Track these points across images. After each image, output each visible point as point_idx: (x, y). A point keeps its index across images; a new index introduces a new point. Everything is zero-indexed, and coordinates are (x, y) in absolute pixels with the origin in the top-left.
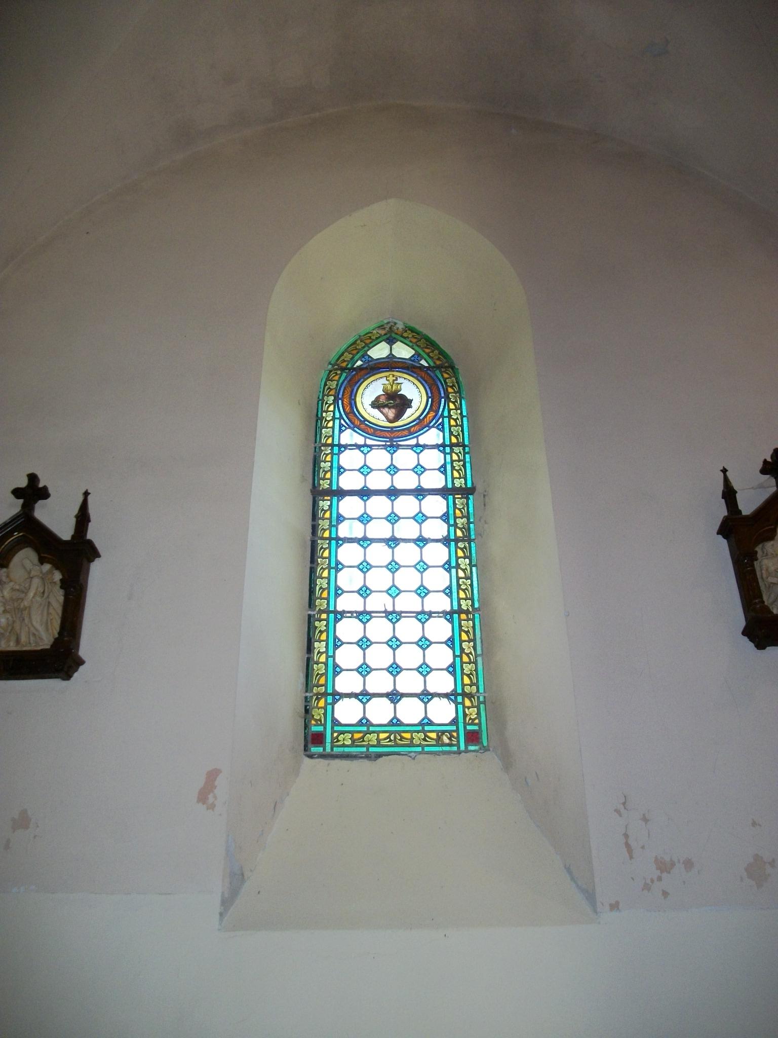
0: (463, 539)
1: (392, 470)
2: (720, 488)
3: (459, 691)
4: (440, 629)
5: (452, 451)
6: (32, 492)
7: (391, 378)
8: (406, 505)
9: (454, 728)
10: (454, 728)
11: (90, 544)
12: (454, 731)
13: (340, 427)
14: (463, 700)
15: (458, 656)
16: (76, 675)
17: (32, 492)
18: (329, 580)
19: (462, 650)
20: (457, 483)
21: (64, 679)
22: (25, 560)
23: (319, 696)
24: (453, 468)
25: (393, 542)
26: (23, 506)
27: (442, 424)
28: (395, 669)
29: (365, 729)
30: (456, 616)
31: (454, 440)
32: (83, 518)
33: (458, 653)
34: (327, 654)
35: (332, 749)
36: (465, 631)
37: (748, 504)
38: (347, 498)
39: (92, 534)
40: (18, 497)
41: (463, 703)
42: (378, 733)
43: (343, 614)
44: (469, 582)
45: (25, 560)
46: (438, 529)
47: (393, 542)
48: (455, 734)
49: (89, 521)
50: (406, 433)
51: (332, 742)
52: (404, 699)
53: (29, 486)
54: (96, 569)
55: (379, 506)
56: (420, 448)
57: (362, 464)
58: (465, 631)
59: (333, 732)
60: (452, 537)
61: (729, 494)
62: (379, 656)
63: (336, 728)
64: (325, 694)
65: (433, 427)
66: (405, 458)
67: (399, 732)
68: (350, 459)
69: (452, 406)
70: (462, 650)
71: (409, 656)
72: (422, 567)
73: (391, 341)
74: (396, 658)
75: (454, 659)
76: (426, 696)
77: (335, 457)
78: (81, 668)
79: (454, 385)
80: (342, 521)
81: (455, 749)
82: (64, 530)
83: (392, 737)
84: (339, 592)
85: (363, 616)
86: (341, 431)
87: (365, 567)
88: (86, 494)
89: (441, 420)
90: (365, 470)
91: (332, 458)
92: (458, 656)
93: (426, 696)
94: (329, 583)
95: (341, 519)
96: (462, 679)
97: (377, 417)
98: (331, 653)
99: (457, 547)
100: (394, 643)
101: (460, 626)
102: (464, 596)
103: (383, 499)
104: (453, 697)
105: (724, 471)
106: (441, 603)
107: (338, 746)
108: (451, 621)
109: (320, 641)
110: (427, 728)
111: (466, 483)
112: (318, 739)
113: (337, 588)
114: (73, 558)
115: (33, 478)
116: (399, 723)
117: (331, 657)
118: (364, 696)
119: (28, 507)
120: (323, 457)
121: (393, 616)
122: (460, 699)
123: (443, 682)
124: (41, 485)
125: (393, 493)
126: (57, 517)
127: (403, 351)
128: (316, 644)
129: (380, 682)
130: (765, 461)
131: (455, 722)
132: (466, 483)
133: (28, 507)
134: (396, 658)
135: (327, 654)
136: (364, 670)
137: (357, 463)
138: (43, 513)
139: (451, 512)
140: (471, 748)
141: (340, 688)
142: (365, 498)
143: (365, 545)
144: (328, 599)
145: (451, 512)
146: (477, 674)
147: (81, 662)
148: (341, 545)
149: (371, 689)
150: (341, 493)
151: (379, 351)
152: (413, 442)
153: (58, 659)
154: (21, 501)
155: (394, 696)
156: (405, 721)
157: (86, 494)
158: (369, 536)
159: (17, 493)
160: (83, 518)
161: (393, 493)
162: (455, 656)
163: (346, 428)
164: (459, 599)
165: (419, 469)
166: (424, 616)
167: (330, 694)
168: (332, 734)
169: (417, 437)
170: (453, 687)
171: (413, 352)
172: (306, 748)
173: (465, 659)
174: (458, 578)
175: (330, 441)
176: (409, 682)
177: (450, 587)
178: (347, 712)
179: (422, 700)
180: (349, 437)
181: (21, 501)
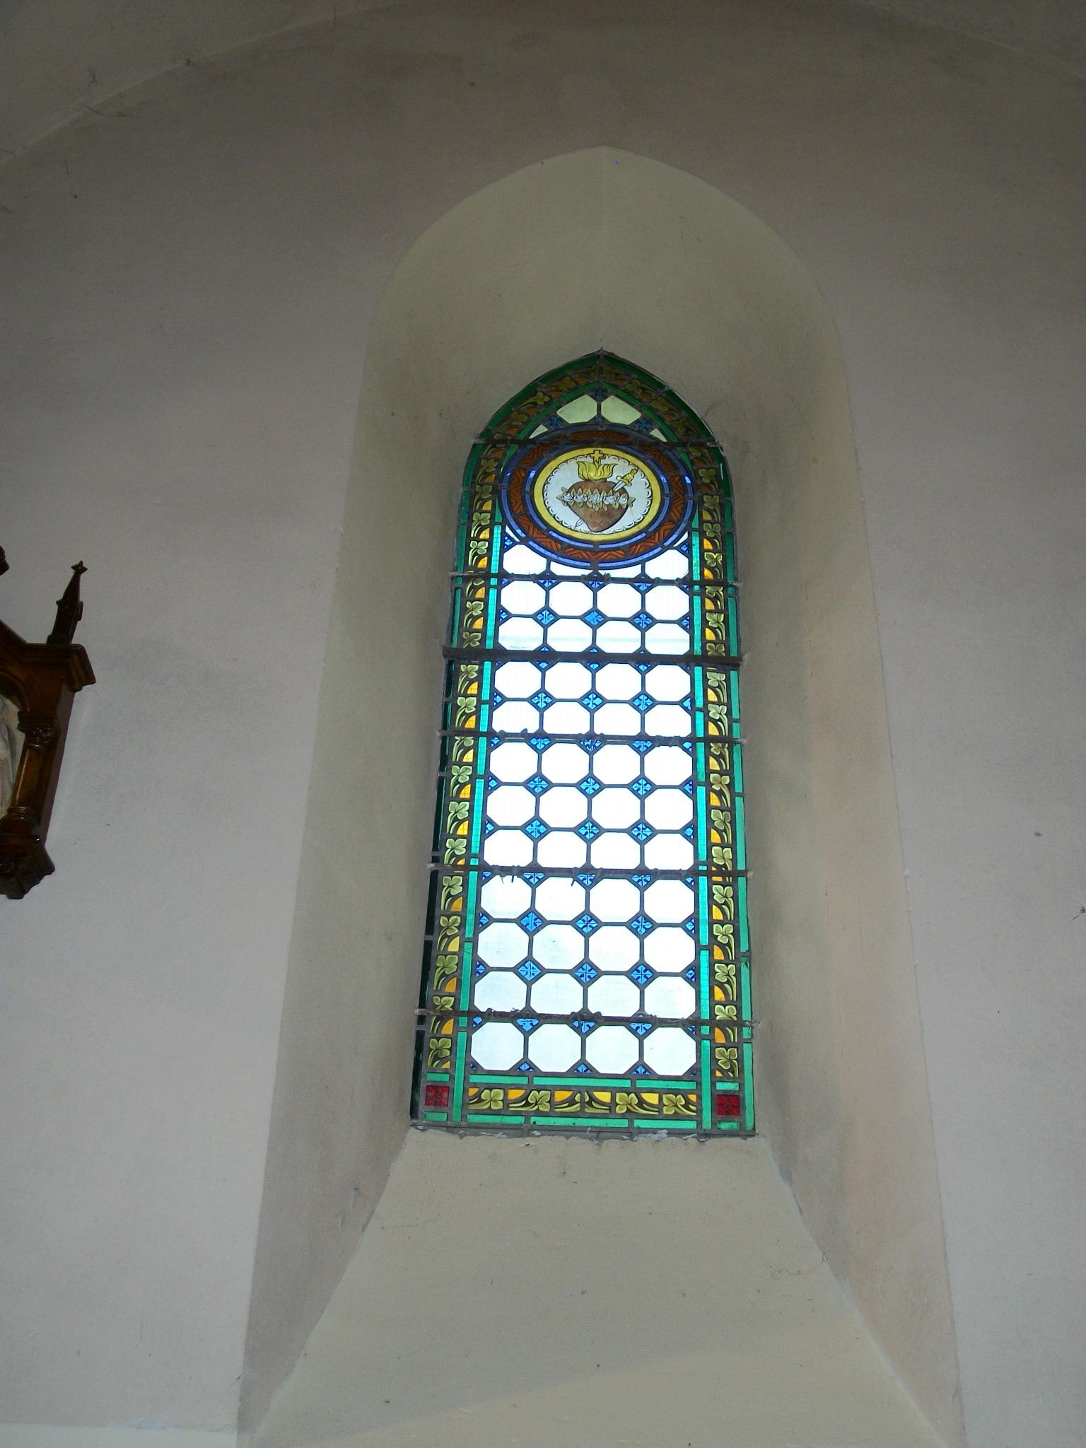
0: (725, 757)
1: (595, 618)
3: (705, 1015)
4: (671, 901)
7: (597, 455)
9: (692, 1086)
10: (692, 1086)
11: (81, 652)
12: (691, 1092)
13: (503, 541)
14: (712, 1031)
15: (705, 948)
16: (35, 889)
18: (486, 605)
19: (712, 937)
20: (722, 1013)
21: (11, 897)
23: (443, 1017)
24: (705, 623)
27: (688, 544)
28: (586, 973)
29: (524, 1080)
30: (703, 881)
31: (713, 731)
32: (70, 608)
33: (704, 940)
34: (462, 936)
35: (463, 1117)
36: (715, 792)
38: (510, 665)
41: (711, 1038)
42: (553, 1089)
43: (505, 737)
44: (727, 780)
46: (675, 722)
47: (591, 742)
48: (693, 1098)
50: (620, 554)
51: (464, 1105)
54: (86, 709)
55: (568, 680)
56: (644, 584)
58: (715, 792)
59: (467, 1085)
60: (696, 577)
62: (559, 947)
63: (474, 1079)
64: (456, 1012)
65: (670, 547)
66: (618, 599)
67: (589, 1090)
69: (706, 516)
70: (712, 937)
71: (613, 949)
72: (642, 925)
73: (599, 396)
75: (697, 954)
76: (642, 1024)
77: (493, 593)
79: (717, 597)
80: (486, 926)
81: (691, 1125)
83: (577, 1098)
84: (484, 920)
85: (540, 740)
86: (504, 549)
87: (538, 784)
88: (79, 569)
89: (685, 536)
90: (546, 617)
91: (487, 593)
92: (705, 948)
93: (642, 1024)
94: (471, 810)
95: (484, 920)
96: (707, 763)
97: (567, 520)
98: (469, 933)
99: (708, 754)
100: (591, 786)
101: (711, 895)
102: (718, 768)
103: (577, 669)
104: (687, 745)
106: (677, 854)
107: (478, 1113)
108: (694, 887)
109: (456, 837)
110: (641, 1084)
111: (734, 860)
112: (439, 1095)
113: (486, 820)
116: (590, 1072)
117: (469, 940)
118: (527, 1020)
120: (455, 753)
121: (591, 742)
122: (705, 1030)
123: (674, 999)
127: (620, 413)
128: (442, 921)
129: (557, 995)
131: (694, 1073)
132: (734, 860)
135: (462, 936)
136: (530, 970)
137: (529, 599)
139: (704, 916)
140: (724, 1126)
141: (491, 858)
142: (544, 665)
144: (468, 838)
145: (704, 916)
146: (739, 983)
148: (497, 746)
149: (539, 1007)
150: (501, 656)
151: (579, 412)
152: (633, 572)
155: (585, 1022)
156: (602, 1069)
157: (79, 569)
160: (70, 608)
161: (588, 875)
162: (699, 948)
163: (515, 543)
164: (710, 846)
165: (643, 621)
166: (643, 743)
167: (463, 1014)
168: (465, 1091)
169: (643, 563)
170: (692, 1009)
171: (638, 415)
172: (414, 1112)
173: (718, 954)
174: (709, 808)
175: (471, 724)
176: (614, 997)
177: (693, 825)
178: (495, 1048)
179: (634, 1032)
180: (522, 559)
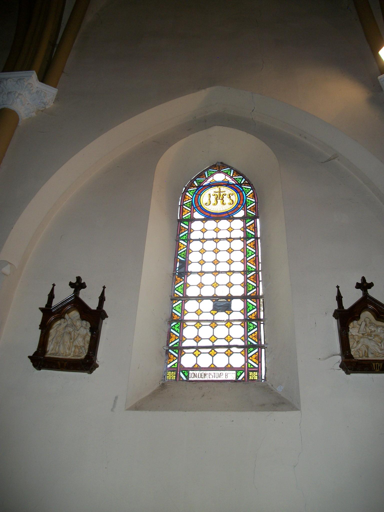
2: (336, 294)
6: (78, 285)
11: (104, 312)
17: (78, 285)
26: (74, 291)
32: (102, 299)
37: (347, 305)
39: (105, 308)
40: (72, 287)
49: (342, 297)
53: (212, 300)
61: (339, 298)
68: (196, 225)
74: (214, 347)
78: (97, 369)
82: (93, 305)
105: (338, 287)
114: (95, 318)
115: (79, 279)
119: (76, 292)
124: (82, 282)
130: (357, 283)
133: (76, 292)
134: (214, 347)
138: (83, 295)
143: (217, 241)
147: (97, 366)
153: (87, 364)
154: (74, 289)
159: (71, 285)
160: (102, 299)
181: (74, 289)
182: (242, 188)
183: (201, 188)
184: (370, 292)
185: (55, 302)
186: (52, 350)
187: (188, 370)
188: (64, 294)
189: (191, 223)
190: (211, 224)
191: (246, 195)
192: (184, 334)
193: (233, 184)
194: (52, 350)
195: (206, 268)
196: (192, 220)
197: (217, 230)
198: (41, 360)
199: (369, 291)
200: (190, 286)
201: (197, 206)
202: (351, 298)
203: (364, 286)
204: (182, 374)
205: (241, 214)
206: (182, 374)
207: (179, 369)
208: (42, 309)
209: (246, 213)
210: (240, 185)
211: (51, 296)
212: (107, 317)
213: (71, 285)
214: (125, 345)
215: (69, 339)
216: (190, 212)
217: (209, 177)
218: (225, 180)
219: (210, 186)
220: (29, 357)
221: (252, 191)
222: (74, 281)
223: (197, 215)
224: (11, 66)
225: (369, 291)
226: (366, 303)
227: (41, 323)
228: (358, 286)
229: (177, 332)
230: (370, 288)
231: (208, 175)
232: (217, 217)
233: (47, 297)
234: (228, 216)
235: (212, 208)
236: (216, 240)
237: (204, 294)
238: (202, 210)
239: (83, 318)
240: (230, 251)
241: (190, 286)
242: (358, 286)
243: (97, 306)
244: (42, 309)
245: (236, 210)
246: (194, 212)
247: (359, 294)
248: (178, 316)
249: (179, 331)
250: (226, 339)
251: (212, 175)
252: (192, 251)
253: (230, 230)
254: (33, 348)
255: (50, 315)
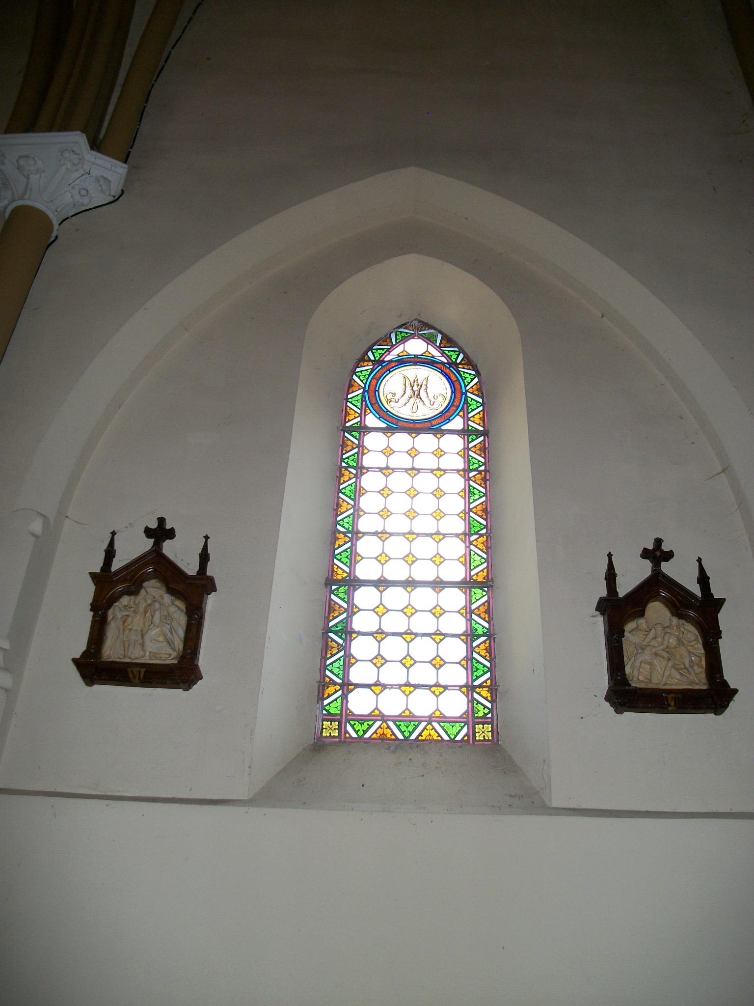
5: (480, 472)
6: (161, 533)
8: (424, 597)
11: (211, 579)
17: (161, 533)
22: (153, 589)
25: (409, 635)
32: (204, 557)
40: (149, 536)
45: (153, 589)
52: (366, 537)
54: (211, 602)
57: (435, 604)
61: (611, 576)
74: (410, 662)
82: (191, 568)
105: (207, 538)
119: (158, 545)
125: (410, 584)
126: (182, 553)
133: (158, 545)
134: (410, 662)
138: (169, 548)
143: (379, 639)
153: (182, 673)
154: (153, 540)
158: (383, 681)
159: (149, 532)
160: (204, 557)
161: (410, 584)
181: (153, 540)
182: (459, 372)
183: (384, 367)
184: (666, 568)
185: (116, 566)
186: (111, 651)
187: (362, 719)
188: (133, 547)
189: (364, 436)
190: (401, 440)
191: (466, 387)
192: (357, 601)
193: (442, 363)
194: (111, 651)
195: (392, 525)
196: (363, 429)
197: (413, 453)
198: (95, 668)
199: (663, 564)
200: (360, 610)
201: (371, 399)
202: (633, 574)
203: (657, 554)
204: (349, 728)
205: (457, 423)
206: (349, 728)
207: (345, 717)
208: (93, 575)
209: (466, 423)
210: (453, 365)
211: (110, 553)
212: (215, 591)
213: (149, 532)
214: (254, 641)
215: (148, 628)
216: (360, 415)
217: (398, 343)
218: (427, 354)
219: (404, 361)
220: (75, 661)
221: (476, 380)
222: (154, 525)
223: (372, 420)
224: (31, 117)
225: (663, 564)
226: (656, 586)
227: (94, 601)
228: (646, 554)
229: (343, 600)
230: (667, 560)
231: (396, 339)
232: (414, 427)
233: (104, 554)
234: (432, 426)
235: (404, 410)
236: (413, 471)
237: (390, 577)
238: (383, 414)
239: (171, 591)
240: (438, 493)
241: (360, 610)
242: (646, 554)
243: (197, 569)
244: (93, 575)
245: (446, 415)
246: (365, 415)
247: (645, 569)
248: (344, 571)
249: (348, 564)
250: (433, 662)
251: (404, 340)
252: (363, 558)
253: (439, 453)
254: (79, 646)
255: (112, 585)
